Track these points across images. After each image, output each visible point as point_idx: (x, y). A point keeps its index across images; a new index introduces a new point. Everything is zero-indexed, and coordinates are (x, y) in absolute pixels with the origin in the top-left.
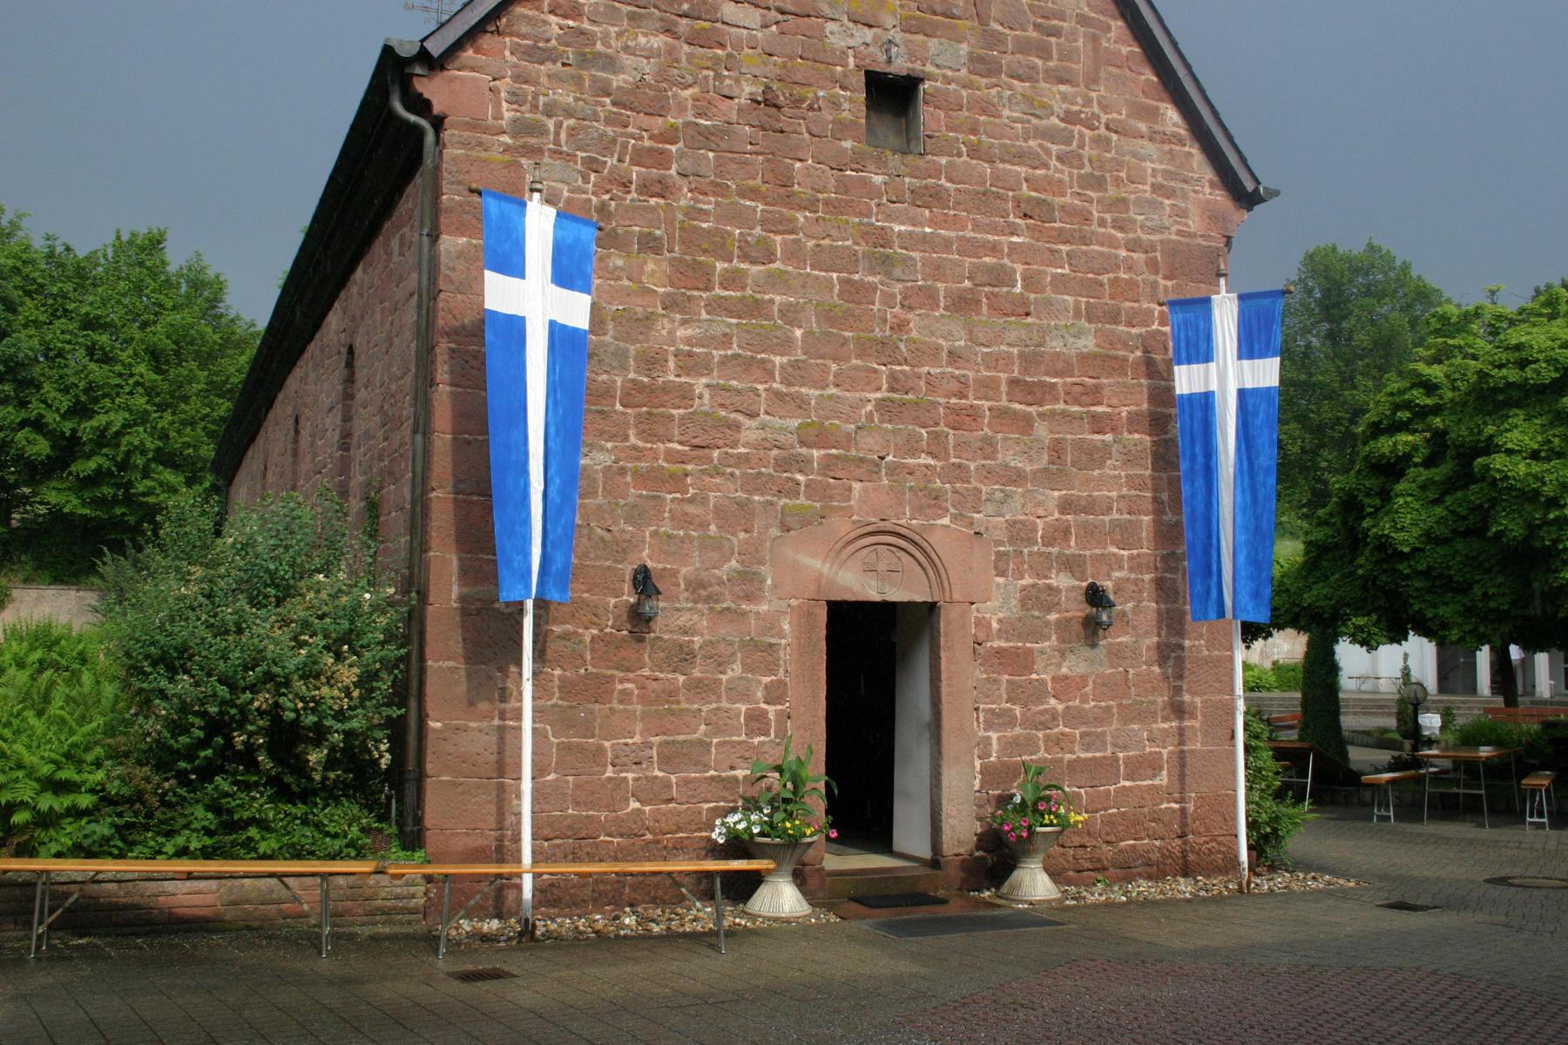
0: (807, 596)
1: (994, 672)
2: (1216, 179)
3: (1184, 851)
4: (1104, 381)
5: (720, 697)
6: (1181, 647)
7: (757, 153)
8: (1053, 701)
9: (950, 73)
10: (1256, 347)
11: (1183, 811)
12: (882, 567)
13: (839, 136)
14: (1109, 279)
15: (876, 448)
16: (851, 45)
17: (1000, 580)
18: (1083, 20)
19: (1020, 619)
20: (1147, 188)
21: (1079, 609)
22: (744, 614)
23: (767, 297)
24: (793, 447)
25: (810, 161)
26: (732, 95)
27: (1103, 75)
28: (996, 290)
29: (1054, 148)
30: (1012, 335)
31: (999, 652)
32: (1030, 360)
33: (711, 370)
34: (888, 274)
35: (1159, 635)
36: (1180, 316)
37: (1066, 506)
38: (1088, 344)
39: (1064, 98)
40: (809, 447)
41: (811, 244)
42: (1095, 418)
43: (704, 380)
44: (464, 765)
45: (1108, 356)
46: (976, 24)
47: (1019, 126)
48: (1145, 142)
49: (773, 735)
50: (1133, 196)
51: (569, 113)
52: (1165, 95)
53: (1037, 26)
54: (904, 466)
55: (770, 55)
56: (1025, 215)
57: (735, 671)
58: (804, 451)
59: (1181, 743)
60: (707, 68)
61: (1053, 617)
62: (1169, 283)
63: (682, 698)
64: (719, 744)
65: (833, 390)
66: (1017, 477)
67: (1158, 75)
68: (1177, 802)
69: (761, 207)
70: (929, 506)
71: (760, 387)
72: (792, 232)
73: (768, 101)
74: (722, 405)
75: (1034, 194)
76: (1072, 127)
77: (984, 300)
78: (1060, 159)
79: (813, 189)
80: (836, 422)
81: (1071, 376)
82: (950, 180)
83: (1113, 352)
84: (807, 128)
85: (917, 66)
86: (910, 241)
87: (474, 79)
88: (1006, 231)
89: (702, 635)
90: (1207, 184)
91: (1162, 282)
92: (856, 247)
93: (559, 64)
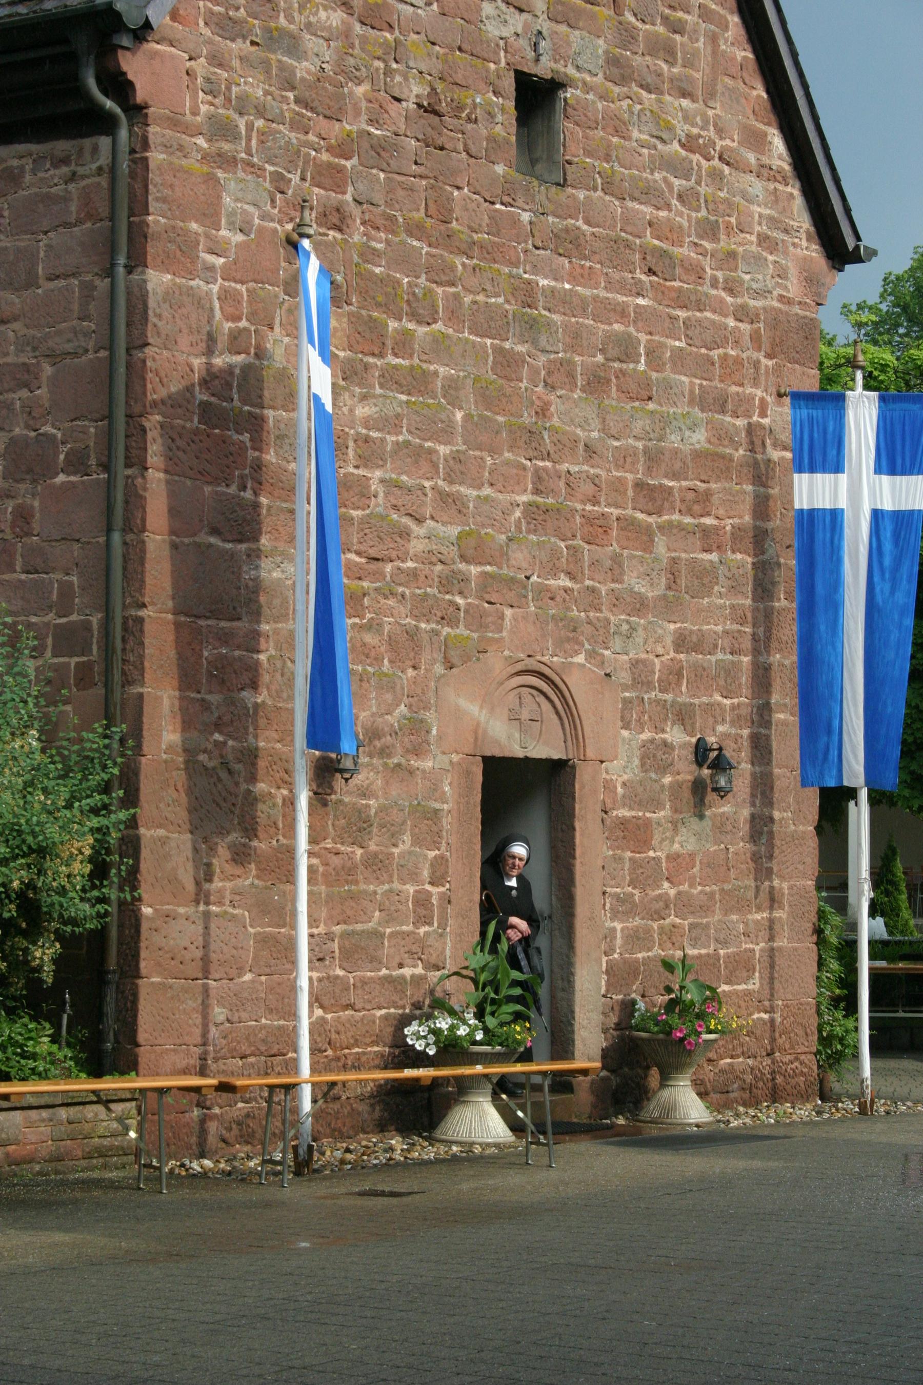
0: (467, 751)
1: (618, 848)
2: (812, 229)
3: (773, 1073)
4: (713, 486)
5: (391, 876)
6: (771, 819)
7: (421, 177)
8: (666, 885)
9: (588, 78)
10: (899, 461)
11: (772, 1021)
12: (525, 715)
13: (492, 159)
14: (719, 356)
15: (524, 565)
16: (504, 35)
17: (625, 733)
18: (705, 13)
19: (641, 783)
20: (754, 238)
21: (687, 771)
22: (411, 772)
23: (432, 368)
24: (454, 563)
25: (466, 190)
26: (402, 97)
27: (719, 87)
28: (624, 366)
29: (676, 182)
30: (639, 426)
31: (623, 823)
32: (653, 458)
33: (385, 461)
34: (534, 342)
35: (753, 804)
36: (805, 412)
37: (681, 642)
38: (699, 438)
39: (687, 118)
40: (468, 562)
41: (468, 299)
42: (706, 532)
43: (378, 474)
44: (173, 963)
45: (717, 454)
46: (612, 13)
47: (645, 151)
48: (752, 178)
49: (436, 924)
50: (741, 249)
51: (261, 112)
52: (773, 118)
53: (665, 19)
54: (547, 589)
55: (433, 44)
56: (650, 270)
57: (406, 843)
58: (462, 566)
59: (771, 939)
60: (379, 59)
61: (667, 780)
62: (770, 363)
63: (360, 877)
64: (392, 935)
65: (487, 491)
66: (640, 606)
67: (768, 92)
68: (766, 1012)
69: (426, 249)
70: (568, 640)
71: (427, 484)
72: (453, 285)
73: (430, 109)
74: (395, 507)
75: (656, 242)
76: (691, 156)
77: (614, 380)
78: (680, 197)
79: (469, 227)
80: (489, 530)
81: (686, 479)
82: (588, 222)
83: (721, 450)
84: (465, 145)
85: (560, 67)
86: (558, 301)
87: (172, 56)
88: (634, 290)
89: (377, 798)
90: (804, 236)
91: (764, 361)
92: (507, 307)
93: (248, 42)
